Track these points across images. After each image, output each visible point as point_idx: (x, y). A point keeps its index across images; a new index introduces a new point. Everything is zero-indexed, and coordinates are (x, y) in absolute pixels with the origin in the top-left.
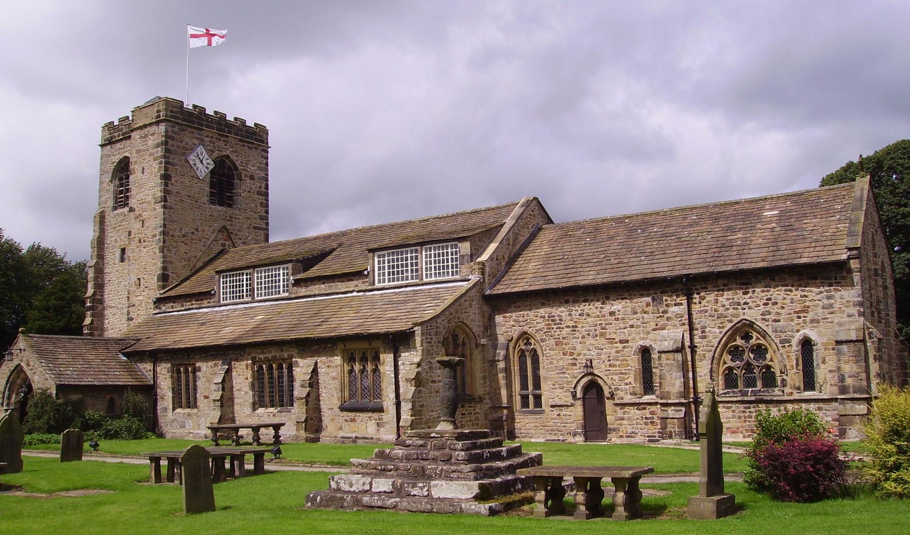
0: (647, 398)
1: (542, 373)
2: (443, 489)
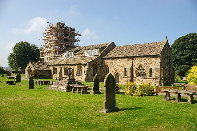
0: (125, 77)
2: (62, 88)
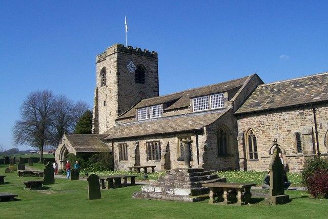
0: (299, 154)
1: (257, 144)
2: (179, 192)
